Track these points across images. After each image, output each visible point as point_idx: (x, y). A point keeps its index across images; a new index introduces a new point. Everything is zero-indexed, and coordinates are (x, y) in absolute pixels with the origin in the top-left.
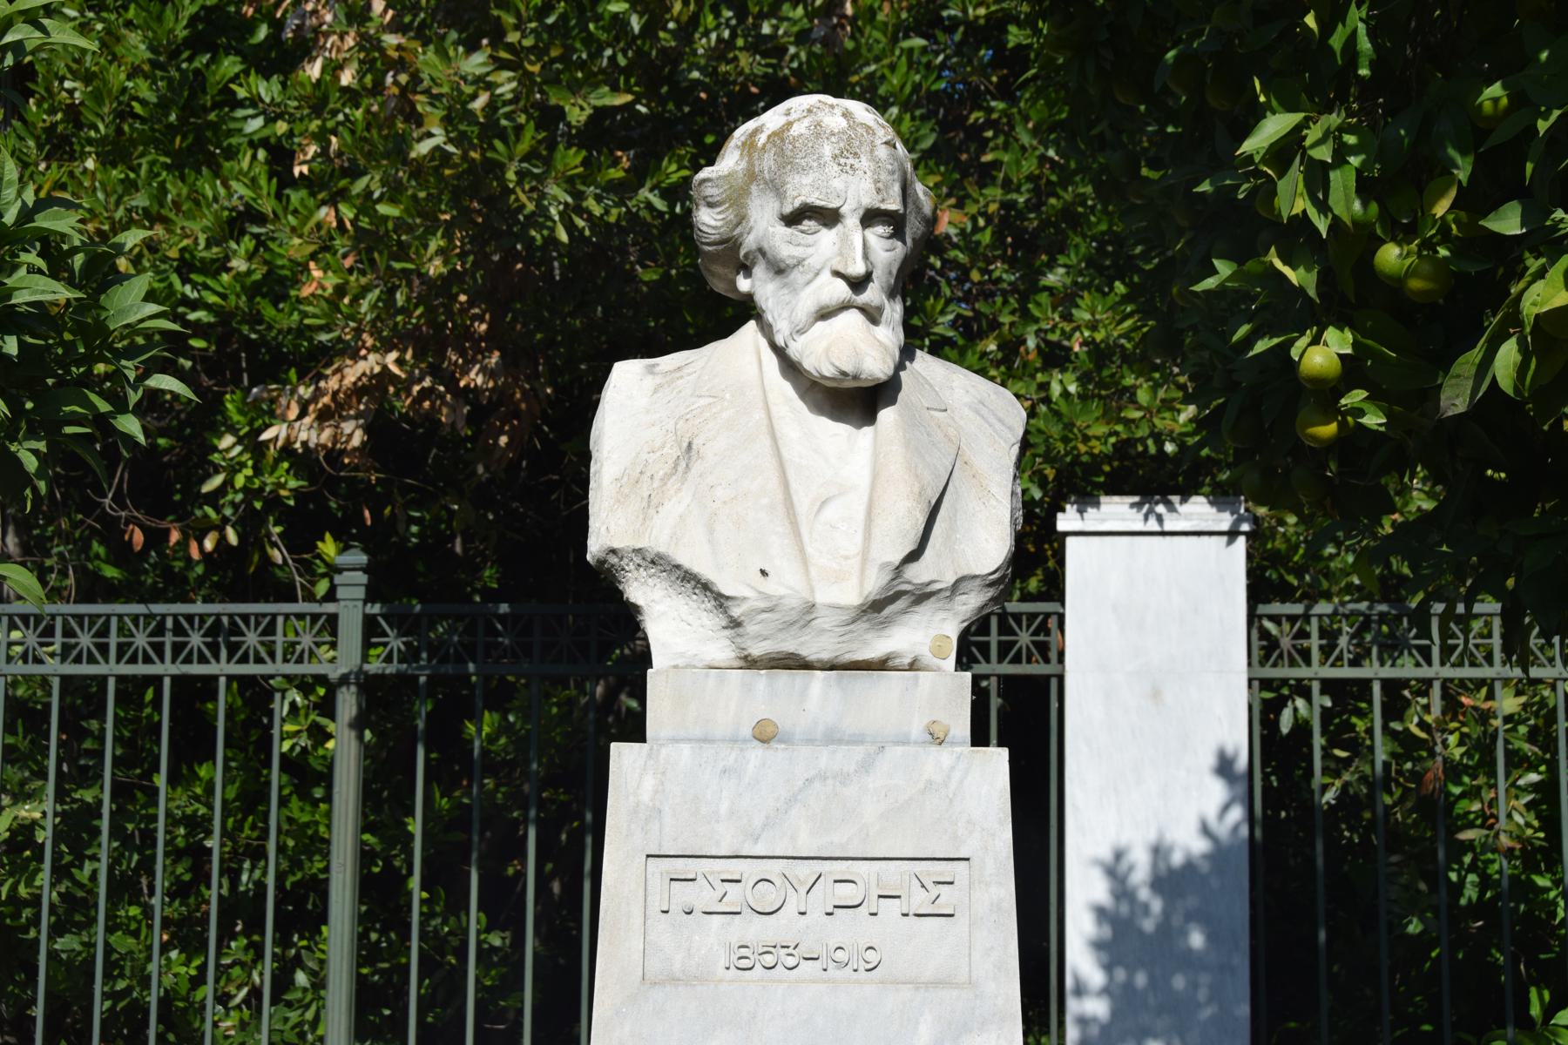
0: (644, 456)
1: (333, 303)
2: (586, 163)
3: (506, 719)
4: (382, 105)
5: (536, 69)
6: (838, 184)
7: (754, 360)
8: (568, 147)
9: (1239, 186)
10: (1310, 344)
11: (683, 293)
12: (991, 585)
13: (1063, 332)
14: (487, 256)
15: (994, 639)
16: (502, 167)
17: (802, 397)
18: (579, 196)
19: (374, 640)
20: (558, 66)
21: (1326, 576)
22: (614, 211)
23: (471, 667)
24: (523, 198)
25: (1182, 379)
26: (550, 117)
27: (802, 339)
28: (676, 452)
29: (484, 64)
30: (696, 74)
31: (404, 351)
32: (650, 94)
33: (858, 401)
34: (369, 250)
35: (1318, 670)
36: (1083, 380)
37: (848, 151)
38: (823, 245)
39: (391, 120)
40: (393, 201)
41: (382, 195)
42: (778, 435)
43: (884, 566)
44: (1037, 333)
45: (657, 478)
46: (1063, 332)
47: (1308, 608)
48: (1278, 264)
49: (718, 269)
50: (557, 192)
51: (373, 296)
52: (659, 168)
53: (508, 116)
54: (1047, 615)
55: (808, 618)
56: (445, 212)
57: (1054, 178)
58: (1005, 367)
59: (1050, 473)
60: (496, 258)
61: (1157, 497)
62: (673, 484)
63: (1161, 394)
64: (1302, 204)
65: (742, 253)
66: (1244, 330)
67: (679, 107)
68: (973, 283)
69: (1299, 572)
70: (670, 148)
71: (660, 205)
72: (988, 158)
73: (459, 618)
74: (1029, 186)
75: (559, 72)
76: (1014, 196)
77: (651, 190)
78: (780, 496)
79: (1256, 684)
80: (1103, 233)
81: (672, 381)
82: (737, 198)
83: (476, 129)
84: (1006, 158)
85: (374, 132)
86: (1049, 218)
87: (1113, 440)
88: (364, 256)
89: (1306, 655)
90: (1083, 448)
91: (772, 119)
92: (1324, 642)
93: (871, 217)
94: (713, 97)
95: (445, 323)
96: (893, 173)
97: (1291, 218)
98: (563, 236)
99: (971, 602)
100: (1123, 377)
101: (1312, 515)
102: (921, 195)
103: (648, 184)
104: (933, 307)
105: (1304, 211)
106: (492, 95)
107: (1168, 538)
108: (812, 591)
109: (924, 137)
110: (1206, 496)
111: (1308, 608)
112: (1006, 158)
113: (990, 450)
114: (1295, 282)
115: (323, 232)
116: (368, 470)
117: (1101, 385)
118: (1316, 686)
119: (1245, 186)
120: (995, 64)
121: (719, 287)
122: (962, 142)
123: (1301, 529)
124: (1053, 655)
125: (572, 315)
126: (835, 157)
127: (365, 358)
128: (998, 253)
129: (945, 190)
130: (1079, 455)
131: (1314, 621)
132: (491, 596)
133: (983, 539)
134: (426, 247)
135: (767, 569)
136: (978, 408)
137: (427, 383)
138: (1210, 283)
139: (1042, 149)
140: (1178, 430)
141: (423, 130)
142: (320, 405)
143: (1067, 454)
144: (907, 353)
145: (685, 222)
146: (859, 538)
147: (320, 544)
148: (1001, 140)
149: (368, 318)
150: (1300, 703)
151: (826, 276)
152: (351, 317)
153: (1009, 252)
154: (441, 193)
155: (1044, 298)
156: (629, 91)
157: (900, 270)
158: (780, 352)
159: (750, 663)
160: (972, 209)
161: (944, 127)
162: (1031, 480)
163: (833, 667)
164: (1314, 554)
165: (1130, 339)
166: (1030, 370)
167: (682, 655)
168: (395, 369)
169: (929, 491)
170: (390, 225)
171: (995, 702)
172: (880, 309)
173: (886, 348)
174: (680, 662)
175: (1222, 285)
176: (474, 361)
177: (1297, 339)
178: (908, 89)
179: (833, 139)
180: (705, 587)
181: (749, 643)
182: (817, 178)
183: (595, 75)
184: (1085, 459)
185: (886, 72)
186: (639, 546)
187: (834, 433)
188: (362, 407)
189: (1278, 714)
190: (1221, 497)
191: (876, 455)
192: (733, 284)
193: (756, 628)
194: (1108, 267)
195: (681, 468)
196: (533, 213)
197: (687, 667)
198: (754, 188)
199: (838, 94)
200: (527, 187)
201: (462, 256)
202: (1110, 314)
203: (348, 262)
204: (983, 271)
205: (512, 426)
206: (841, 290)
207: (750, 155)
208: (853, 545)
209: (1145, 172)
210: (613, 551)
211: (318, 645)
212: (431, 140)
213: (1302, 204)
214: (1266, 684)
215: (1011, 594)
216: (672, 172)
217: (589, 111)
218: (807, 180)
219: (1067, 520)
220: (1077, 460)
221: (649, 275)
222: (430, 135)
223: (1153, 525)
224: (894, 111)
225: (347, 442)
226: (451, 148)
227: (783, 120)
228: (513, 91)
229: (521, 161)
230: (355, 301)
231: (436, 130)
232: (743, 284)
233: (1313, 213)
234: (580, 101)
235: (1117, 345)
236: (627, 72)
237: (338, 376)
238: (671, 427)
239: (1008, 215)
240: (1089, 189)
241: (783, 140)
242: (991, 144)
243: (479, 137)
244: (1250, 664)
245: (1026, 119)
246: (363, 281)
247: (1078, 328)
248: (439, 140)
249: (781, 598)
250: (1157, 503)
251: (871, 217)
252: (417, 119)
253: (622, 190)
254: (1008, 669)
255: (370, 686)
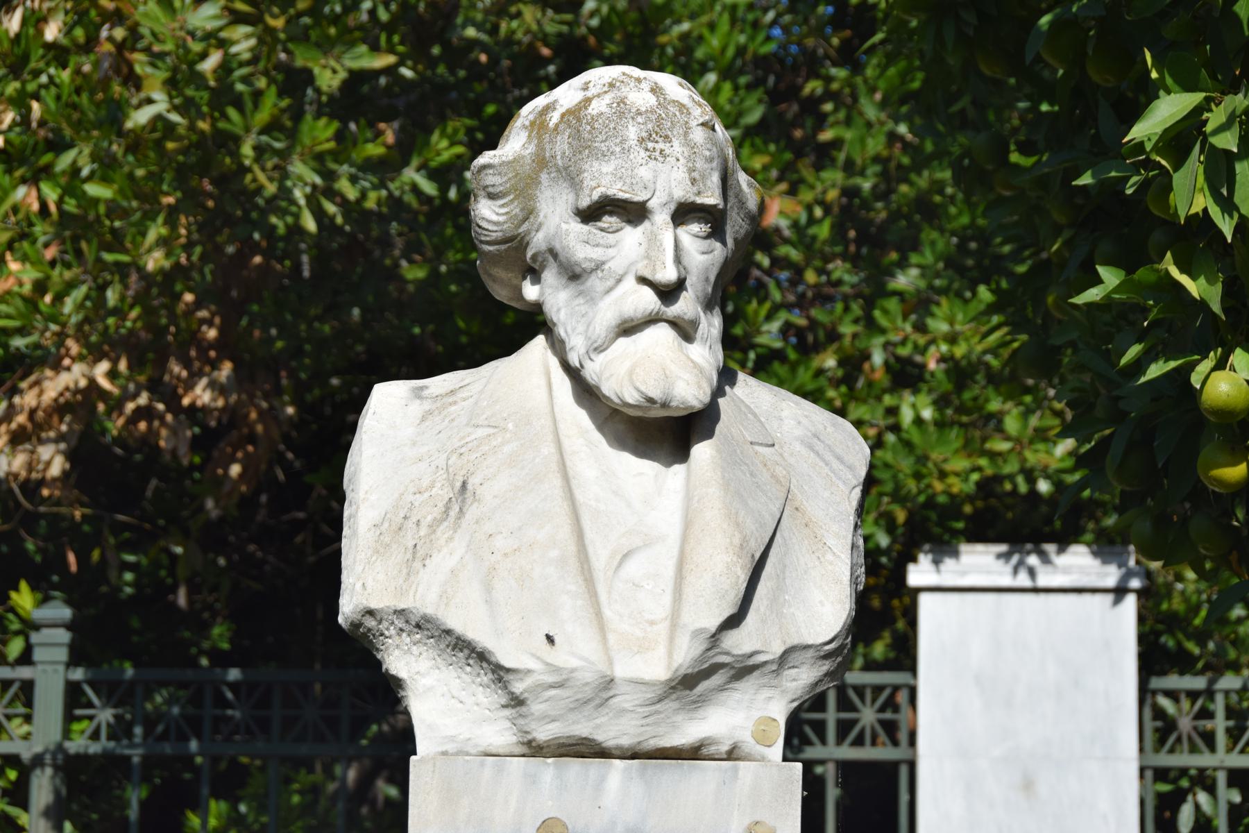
0: (411, 498)
1: (31, 303)
2: (339, 136)
3: (236, 810)
4: (97, 64)
5: (278, 23)
6: (645, 173)
7: (543, 382)
8: (318, 116)
9: (1127, 179)
10: (1215, 369)
11: (456, 295)
12: (826, 657)
13: (916, 346)
14: (219, 249)
15: (831, 716)
16: (237, 140)
17: (600, 428)
18: (329, 176)
19: (78, 712)
20: (306, 20)
21: (1234, 643)
22: (373, 196)
23: (194, 745)
24: (262, 177)
25: (1058, 406)
26: (295, 82)
27: (600, 359)
28: (447, 493)
29: (215, 17)
30: (471, 32)
31: (115, 362)
32: (417, 53)
33: (667, 433)
34: (75, 239)
35: (1223, 758)
36: (941, 403)
37: (657, 133)
38: (627, 245)
39: (105, 84)
40: (105, 180)
41: (92, 173)
42: (571, 473)
43: (697, 633)
44: (886, 345)
45: (424, 524)
46: (916, 346)
47: (1212, 682)
48: (1175, 272)
49: (499, 272)
50: (303, 172)
51: (80, 293)
52: (427, 143)
53: (245, 80)
54: (896, 688)
55: (605, 695)
56: (167, 194)
57: (906, 160)
58: (842, 391)
59: (901, 516)
60: (230, 249)
61: (1029, 546)
62: (443, 532)
63: (1034, 421)
64: (1202, 202)
65: (529, 254)
66: (1134, 351)
67: (452, 71)
68: (809, 286)
69: (1201, 637)
70: (443, 119)
71: (429, 188)
72: (826, 135)
73: (183, 685)
74: (877, 168)
75: (307, 28)
76: (858, 180)
77: (418, 170)
78: (572, 548)
79: (1149, 774)
80: (965, 228)
81: (444, 407)
82: (523, 188)
83: (205, 95)
84: (848, 135)
85: (85, 98)
86: (899, 208)
87: (975, 477)
88: (69, 246)
89: (1209, 739)
90: (938, 486)
91: (567, 94)
92: (1231, 723)
93: (683, 213)
94: (494, 61)
95: (167, 327)
96: (711, 160)
97: (1189, 219)
98: (310, 224)
99: (803, 678)
100: (987, 401)
101: (1215, 571)
102: (744, 186)
103: (415, 162)
104: (756, 312)
105: (1205, 210)
106: (226, 54)
107: (1043, 596)
108: (611, 663)
109: (750, 110)
110: (1088, 544)
111: (1212, 682)
112: (848, 135)
113: (827, 494)
114: (1195, 294)
115: (21, 216)
116: (71, 505)
117: (961, 410)
118: (1221, 778)
119: (1134, 179)
120: (837, 22)
121: (501, 294)
122: (796, 116)
123: (1203, 585)
124: (903, 736)
125: (321, 319)
126: (641, 141)
127: (68, 369)
128: (838, 249)
129: (774, 173)
130: (934, 495)
131: (1220, 700)
132: (221, 660)
133: (817, 599)
134: (144, 234)
135: (556, 639)
136: (813, 441)
137: (143, 400)
138: (1093, 295)
139: (890, 125)
140: (1054, 465)
141: (143, 95)
142: (14, 426)
143: (920, 492)
144: (726, 376)
145: (460, 213)
146: (667, 599)
147: (13, 595)
148: (841, 115)
149: (74, 320)
150: (1203, 797)
151: (630, 282)
152: (53, 318)
153: (852, 248)
154: (163, 170)
155: (893, 304)
156: (391, 50)
157: (719, 276)
158: (574, 374)
159: (534, 750)
160: (807, 196)
161: (775, 98)
162: (876, 522)
163: (635, 755)
164: (1219, 616)
165: (996, 355)
166: (876, 391)
167: (452, 739)
168: (105, 383)
169: (753, 543)
170: (102, 209)
171: (832, 793)
172: (695, 324)
173: (701, 370)
174: (450, 747)
175: (1107, 296)
176: (200, 374)
177: (1198, 362)
178: (730, 52)
179: (640, 119)
180: (481, 657)
181: (533, 725)
182: (619, 166)
183: (350, 31)
184: (942, 499)
185: (706, 32)
186: (402, 606)
187: (638, 472)
188: (64, 428)
189: (1175, 811)
190: (1107, 546)
191: (688, 498)
192: (518, 291)
193: (543, 707)
194: (970, 269)
195: (456, 508)
196: (275, 198)
197: (460, 753)
198: (544, 177)
199: (645, 65)
200: (269, 164)
201: (188, 247)
202: (973, 325)
203: (50, 253)
204: (821, 271)
205: (247, 454)
206: (648, 300)
207: (540, 137)
208: (660, 607)
209: (1015, 157)
210: (370, 613)
211: (9, 717)
212: (151, 108)
213: (1202, 202)
214: (1161, 774)
215: (852, 662)
216: (443, 149)
217: (343, 75)
218: (607, 168)
219: (920, 573)
220: (930, 503)
221: (414, 273)
222: (150, 101)
223: (1023, 580)
224: (711, 78)
225: (45, 470)
226: (175, 117)
227: (579, 96)
228: (251, 50)
229: (261, 133)
230: (59, 299)
231: (159, 96)
232: (531, 292)
233: (1215, 212)
234: (332, 63)
235: (980, 362)
236: (390, 28)
237: (36, 391)
238: (441, 462)
239: (850, 205)
240: (947, 175)
241: (579, 120)
242: (831, 119)
243: (209, 104)
244: (1141, 750)
245: (872, 90)
246: (68, 275)
247: (933, 341)
248: (161, 105)
249: (573, 670)
250: (1029, 553)
251: (683, 213)
252: (133, 81)
253: (384, 168)
254: (848, 752)
255: (71, 768)
